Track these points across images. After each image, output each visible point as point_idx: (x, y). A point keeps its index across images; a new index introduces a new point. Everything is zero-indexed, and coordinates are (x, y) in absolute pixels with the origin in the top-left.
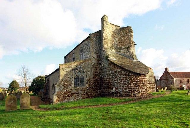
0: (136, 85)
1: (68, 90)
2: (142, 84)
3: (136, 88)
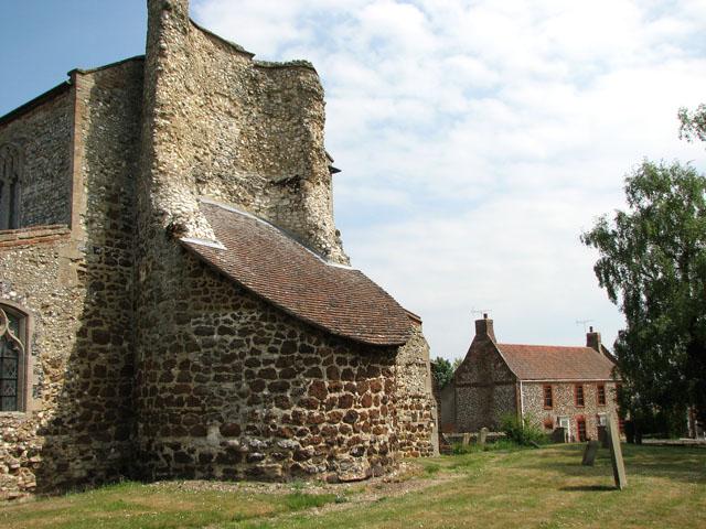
0: (344, 412)
3: (344, 430)
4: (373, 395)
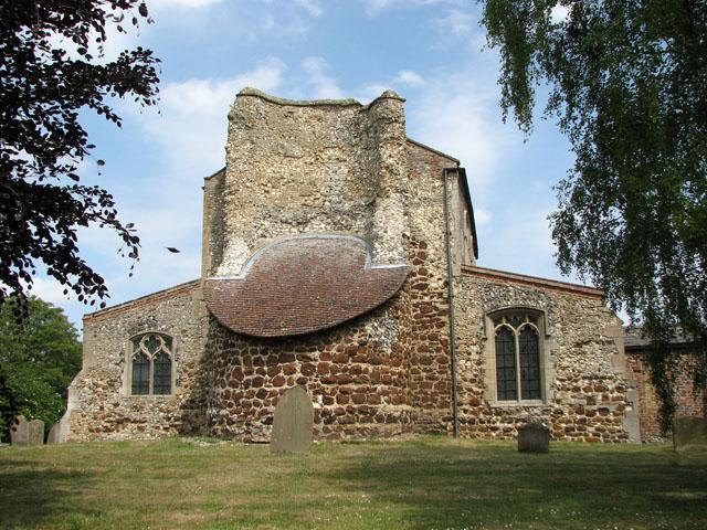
0: (256, 390)
1: (108, 406)
2: (285, 386)
3: (257, 404)
4: (287, 377)
